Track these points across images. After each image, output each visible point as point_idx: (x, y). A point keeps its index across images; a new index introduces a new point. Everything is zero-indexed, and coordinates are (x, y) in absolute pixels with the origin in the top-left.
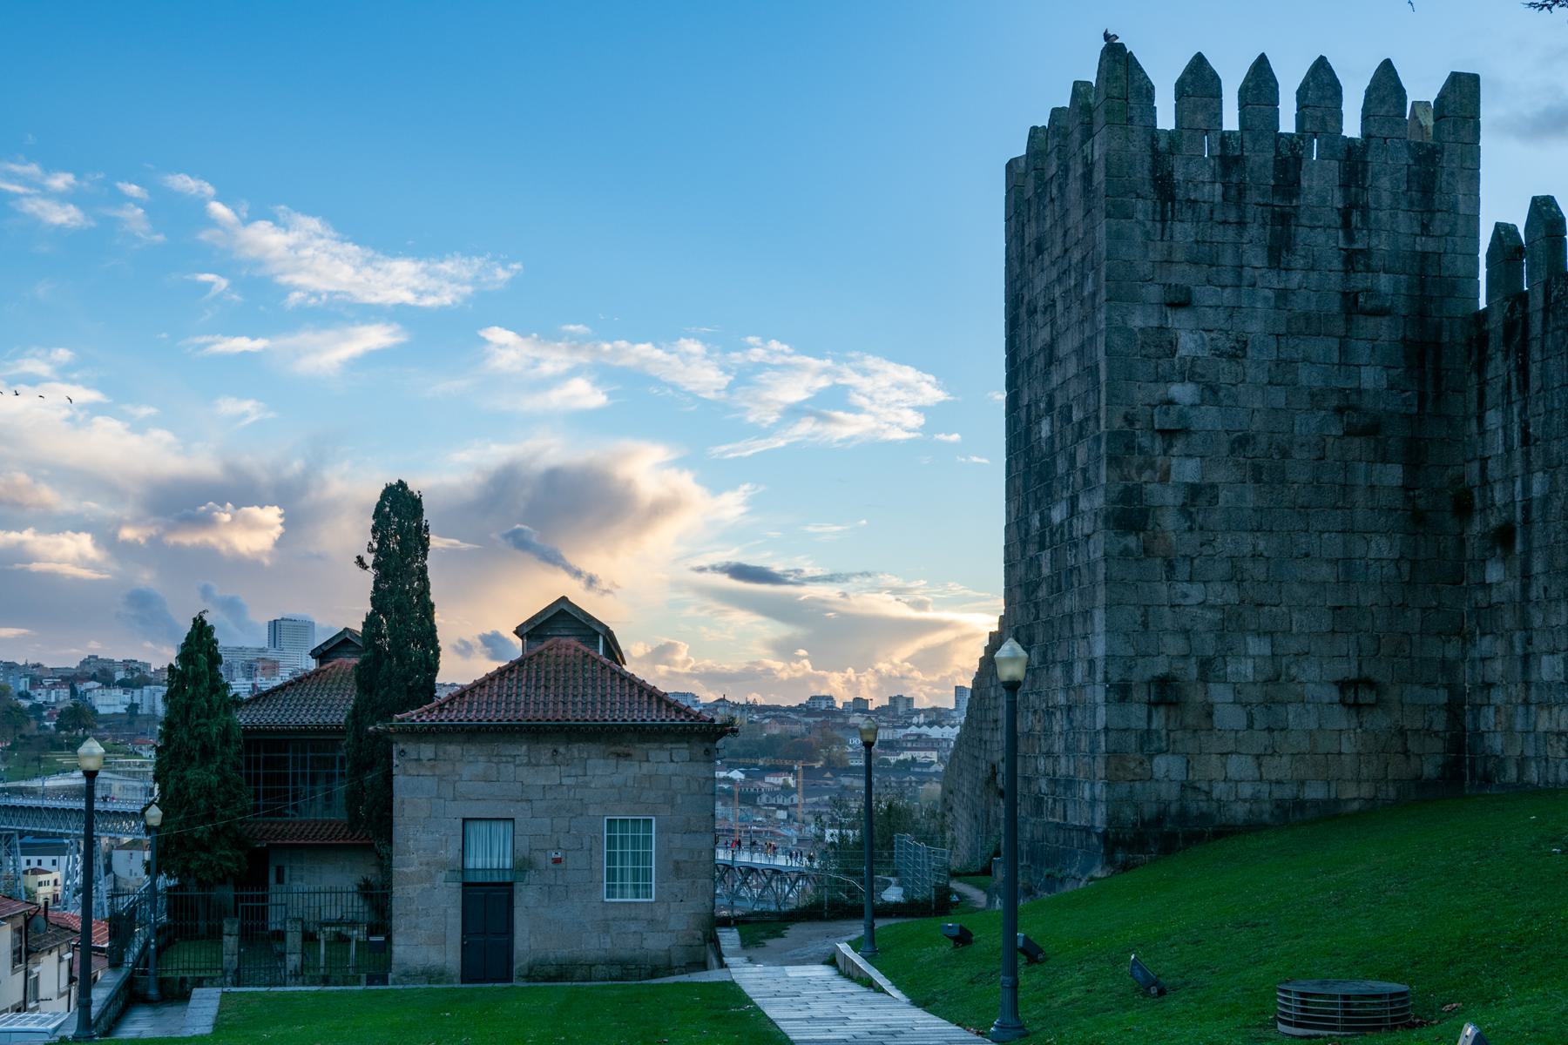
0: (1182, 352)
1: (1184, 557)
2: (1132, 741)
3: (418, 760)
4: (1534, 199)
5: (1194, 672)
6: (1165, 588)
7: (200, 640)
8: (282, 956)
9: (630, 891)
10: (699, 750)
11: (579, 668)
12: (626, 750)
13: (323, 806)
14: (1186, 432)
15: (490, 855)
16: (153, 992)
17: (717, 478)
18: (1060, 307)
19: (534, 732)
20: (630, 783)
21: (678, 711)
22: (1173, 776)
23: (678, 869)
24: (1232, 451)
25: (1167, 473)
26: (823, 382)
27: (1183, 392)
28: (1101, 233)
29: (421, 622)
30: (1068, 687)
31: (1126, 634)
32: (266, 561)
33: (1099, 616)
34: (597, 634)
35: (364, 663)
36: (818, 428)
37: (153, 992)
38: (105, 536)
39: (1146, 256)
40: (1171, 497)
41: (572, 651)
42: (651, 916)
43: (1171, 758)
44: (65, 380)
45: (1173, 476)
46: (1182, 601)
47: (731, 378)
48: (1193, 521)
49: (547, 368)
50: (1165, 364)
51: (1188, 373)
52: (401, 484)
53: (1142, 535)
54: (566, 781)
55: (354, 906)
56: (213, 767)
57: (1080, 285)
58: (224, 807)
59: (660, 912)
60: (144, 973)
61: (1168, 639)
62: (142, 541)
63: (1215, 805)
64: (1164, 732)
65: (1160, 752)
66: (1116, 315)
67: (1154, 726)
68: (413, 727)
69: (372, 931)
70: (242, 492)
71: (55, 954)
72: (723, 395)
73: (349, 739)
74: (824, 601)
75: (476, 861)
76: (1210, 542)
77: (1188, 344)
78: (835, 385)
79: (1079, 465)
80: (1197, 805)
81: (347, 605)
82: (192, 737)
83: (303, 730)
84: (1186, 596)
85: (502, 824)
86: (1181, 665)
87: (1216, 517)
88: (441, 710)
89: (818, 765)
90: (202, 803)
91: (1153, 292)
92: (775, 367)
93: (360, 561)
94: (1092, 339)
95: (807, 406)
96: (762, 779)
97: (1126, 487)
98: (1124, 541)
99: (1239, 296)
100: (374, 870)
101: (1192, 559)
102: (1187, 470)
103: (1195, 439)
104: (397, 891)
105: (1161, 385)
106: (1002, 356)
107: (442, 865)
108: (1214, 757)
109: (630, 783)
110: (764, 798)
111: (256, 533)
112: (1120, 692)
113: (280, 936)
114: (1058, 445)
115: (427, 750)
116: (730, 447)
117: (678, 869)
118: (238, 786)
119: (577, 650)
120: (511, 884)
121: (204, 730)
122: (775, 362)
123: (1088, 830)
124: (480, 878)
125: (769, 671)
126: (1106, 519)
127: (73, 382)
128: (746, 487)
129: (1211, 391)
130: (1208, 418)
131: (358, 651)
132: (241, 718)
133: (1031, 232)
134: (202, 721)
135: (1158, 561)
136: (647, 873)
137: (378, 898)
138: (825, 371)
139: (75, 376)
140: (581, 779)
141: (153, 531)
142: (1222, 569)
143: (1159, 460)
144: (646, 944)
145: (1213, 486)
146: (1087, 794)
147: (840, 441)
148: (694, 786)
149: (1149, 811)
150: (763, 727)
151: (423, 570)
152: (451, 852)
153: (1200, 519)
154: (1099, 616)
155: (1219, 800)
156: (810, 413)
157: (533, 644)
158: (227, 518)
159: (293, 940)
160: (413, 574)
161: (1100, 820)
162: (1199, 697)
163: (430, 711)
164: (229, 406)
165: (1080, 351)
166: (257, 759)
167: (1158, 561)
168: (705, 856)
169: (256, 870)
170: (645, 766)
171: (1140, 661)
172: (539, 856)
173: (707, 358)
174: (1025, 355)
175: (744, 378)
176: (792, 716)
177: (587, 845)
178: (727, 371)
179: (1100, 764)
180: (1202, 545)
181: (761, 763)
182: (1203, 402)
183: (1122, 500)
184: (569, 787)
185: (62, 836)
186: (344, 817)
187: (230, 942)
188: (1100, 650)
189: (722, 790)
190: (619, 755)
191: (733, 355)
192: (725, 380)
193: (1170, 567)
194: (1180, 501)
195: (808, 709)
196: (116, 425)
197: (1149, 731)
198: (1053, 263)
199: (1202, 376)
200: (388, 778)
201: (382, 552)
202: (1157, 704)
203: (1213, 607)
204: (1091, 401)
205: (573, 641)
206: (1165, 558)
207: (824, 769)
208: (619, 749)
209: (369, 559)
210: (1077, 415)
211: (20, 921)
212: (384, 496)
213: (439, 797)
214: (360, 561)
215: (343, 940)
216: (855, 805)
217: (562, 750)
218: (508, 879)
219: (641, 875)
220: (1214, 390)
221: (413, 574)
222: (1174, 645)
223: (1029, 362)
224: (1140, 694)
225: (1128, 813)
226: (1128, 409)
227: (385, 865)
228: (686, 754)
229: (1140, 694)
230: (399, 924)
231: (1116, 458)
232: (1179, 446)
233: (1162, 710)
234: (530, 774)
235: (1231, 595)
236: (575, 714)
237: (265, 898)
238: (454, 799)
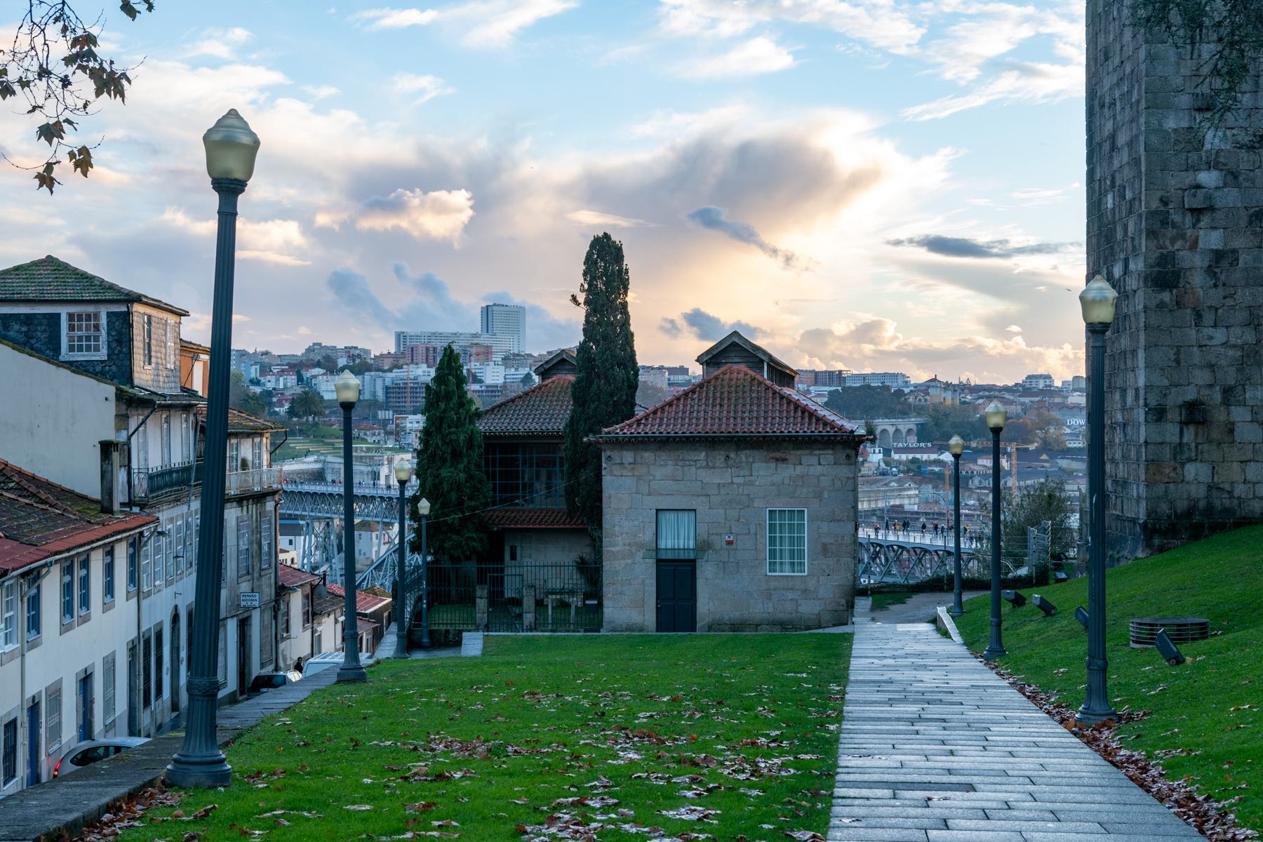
0: (1208, 146)
1: (1210, 307)
2: (1167, 453)
5: (1218, 397)
6: (1194, 332)
8: (520, 616)
9: (787, 567)
10: (842, 455)
11: (747, 389)
12: (783, 456)
13: (546, 497)
14: (1211, 209)
15: (678, 538)
16: (425, 640)
17: (917, 141)
18: (1118, 107)
19: (711, 442)
20: (787, 481)
21: (825, 424)
22: (1200, 479)
23: (825, 550)
24: (1250, 223)
25: (1196, 242)
26: (1026, 32)
27: (1208, 178)
28: (1142, 54)
29: (623, 349)
30: (1124, 409)
31: (1162, 369)
32: (456, 246)
33: (1141, 354)
34: (762, 361)
35: (579, 382)
36: (1022, 82)
37: (425, 640)
38: (307, 226)
39: (1178, 71)
40: (1199, 261)
41: (742, 375)
42: (806, 584)
43: (1198, 464)
44: (246, 62)
45: (1201, 244)
46: (1208, 343)
47: (924, 31)
48: (1217, 279)
49: (726, 29)
50: (1193, 156)
51: (1212, 163)
52: (606, 236)
53: (1174, 291)
54: (736, 480)
55: (572, 579)
56: (461, 466)
57: (1130, 92)
58: (470, 499)
59: (811, 584)
60: (419, 626)
61: (1197, 372)
62: (337, 227)
63: (1236, 502)
64: (1193, 445)
65: (1190, 460)
66: (1154, 121)
67: (1185, 440)
68: (617, 438)
69: (587, 596)
70: (430, 177)
71: (332, 616)
72: (916, 50)
73: (568, 442)
74: (1034, 274)
75: (667, 542)
76: (1231, 296)
77: (1213, 140)
78: (1038, 35)
79: (1130, 234)
80: (1220, 501)
81: (560, 322)
82: (445, 443)
83: (531, 436)
84: (1211, 338)
85: (242, 227)
86: (1207, 392)
87: (1237, 275)
88: (639, 425)
89: (1032, 447)
90: (454, 495)
91: (1184, 100)
92: (971, 18)
93: (574, 299)
94: (1137, 136)
95: (1010, 59)
96: (975, 462)
97: (1162, 254)
98: (1160, 297)
99: (1256, 99)
100: (588, 550)
101: (1217, 309)
102: (1212, 239)
103: (1219, 215)
104: (607, 565)
105: (1191, 173)
107: (641, 546)
108: (1235, 465)
109: (787, 481)
110: (976, 481)
111: (444, 216)
112: (1158, 414)
113: (518, 602)
114: (1117, 217)
115: (628, 456)
116: (924, 107)
117: (825, 550)
118: (480, 481)
119: (746, 374)
120: (694, 561)
121: (453, 437)
122: (970, 11)
123: (1134, 521)
124: (670, 556)
125: (979, 349)
126: (1146, 279)
127: (255, 64)
128: (946, 151)
129: (1232, 176)
130: (1230, 198)
131: (573, 370)
132: (481, 426)
133: (1102, 40)
134: (452, 430)
135: (1188, 311)
136: (801, 552)
137: (591, 572)
138: (1027, 19)
139: (254, 56)
140: (748, 479)
141: (345, 216)
142: (1242, 316)
143: (1189, 232)
144: (801, 609)
145: (1234, 251)
146: (1135, 494)
147: (1045, 97)
148: (838, 484)
149: (1181, 506)
150: (976, 408)
151: (625, 305)
152: (648, 536)
153: (1223, 277)
154: (1141, 354)
155: (1239, 498)
156: (1012, 67)
157: (711, 370)
158: (416, 202)
159: (529, 603)
160: (617, 309)
161: (1142, 513)
162: (1223, 417)
163: (630, 426)
164: (407, 83)
165: (1131, 144)
166: (494, 460)
167: (1188, 311)
168: (848, 539)
169: (494, 548)
170: (799, 468)
171: (1173, 390)
172: (715, 539)
173: (895, 10)
174: (1097, 139)
175: (938, 29)
176: (1007, 396)
177: (752, 531)
178: (919, 24)
179: (1142, 470)
180: (1225, 298)
181: (974, 444)
182: (1225, 185)
183: (1158, 264)
185: (296, 517)
186: (564, 506)
187: (482, 604)
188: (1141, 382)
189: (933, 473)
191: (924, 5)
192: (918, 33)
193: (1198, 316)
194: (1206, 264)
195: (1023, 390)
196: (299, 107)
197: (1180, 444)
198: (1115, 70)
199: (1225, 165)
200: (599, 478)
201: (591, 290)
202: (1187, 423)
203: (1234, 346)
204: (1136, 186)
205: (743, 367)
206: (1194, 309)
207: (1039, 451)
208: (778, 455)
209: (581, 298)
210: (1129, 195)
211: (308, 590)
212: (593, 246)
213: (637, 493)
214: (574, 299)
215: (564, 605)
217: (732, 455)
218: (692, 556)
219: (796, 555)
220: (1235, 175)
221: (617, 309)
222: (1202, 377)
223: (1100, 145)
224: (1173, 415)
225: (1164, 508)
226: (1163, 193)
227: (597, 545)
228: (831, 458)
229: (1173, 415)
230: (608, 591)
231: (1154, 232)
232: (1205, 220)
233: (1192, 428)
234: (707, 476)
235: (1250, 337)
236: (744, 427)
237: (502, 570)
238: (649, 494)
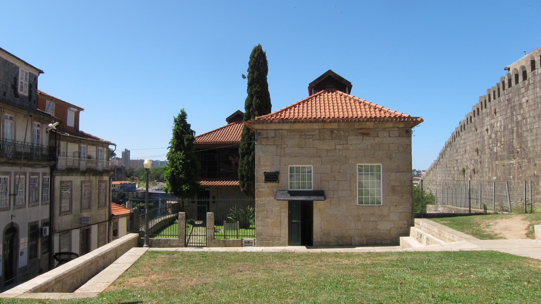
3: (267, 138)
7: (182, 128)
170: (377, 139)
184: (339, 150)
190: (363, 134)
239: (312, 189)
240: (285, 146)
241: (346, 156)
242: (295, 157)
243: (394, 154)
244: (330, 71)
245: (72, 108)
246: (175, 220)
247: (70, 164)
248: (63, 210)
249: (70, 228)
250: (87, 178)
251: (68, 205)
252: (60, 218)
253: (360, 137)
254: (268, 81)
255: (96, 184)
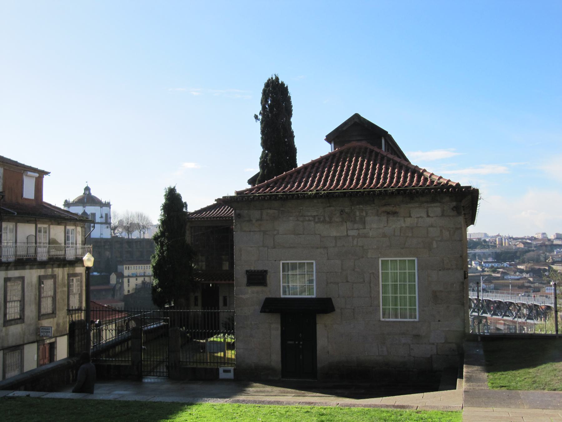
4: (357, 116)
7: (173, 202)
54: (351, 233)
93: (256, 117)
106: (204, 206)
140: (361, 231)
170: (408, 220)
184: (353, 237)
216: (530, 249)
239: (314, 296)
240: (275, 232)
241: (363, 247)
242: (291, 247)
243: (434, 243)
244: (357, 116)
245: (30, 173)
246: (129, 340)
247: (22, 252)
248: (8, 317)
249: (22, 343)
250: (49, 271)
251: (18, 310)
252: (4, 329)
253: (384, 218)
254: (293, 127)
255: (63, 277)
